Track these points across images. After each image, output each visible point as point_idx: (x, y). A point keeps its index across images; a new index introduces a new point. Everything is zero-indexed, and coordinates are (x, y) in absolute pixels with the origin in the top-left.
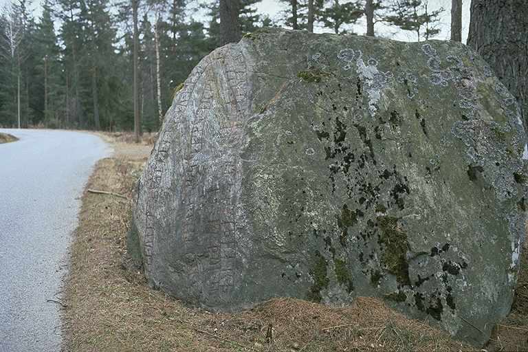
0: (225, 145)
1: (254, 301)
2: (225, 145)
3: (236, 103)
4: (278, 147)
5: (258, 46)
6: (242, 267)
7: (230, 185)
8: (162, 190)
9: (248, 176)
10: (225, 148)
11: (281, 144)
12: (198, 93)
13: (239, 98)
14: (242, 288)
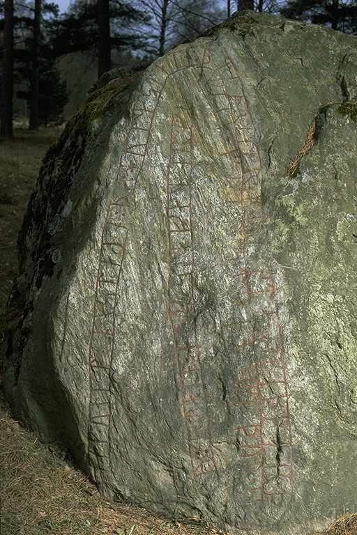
0: (238, 236)
1: (329, 516)
2: (238, 236)
3: (241, 155)
4: (340, 243)
5: (254, 49)
6: (305, 460)
7: (268, 314)
8: (123, 320)
9: (296, 298)
10: (240, 241)
11: (344, 239)
12: (162, 133)
13: (246, 148)
14: (307, 495)
